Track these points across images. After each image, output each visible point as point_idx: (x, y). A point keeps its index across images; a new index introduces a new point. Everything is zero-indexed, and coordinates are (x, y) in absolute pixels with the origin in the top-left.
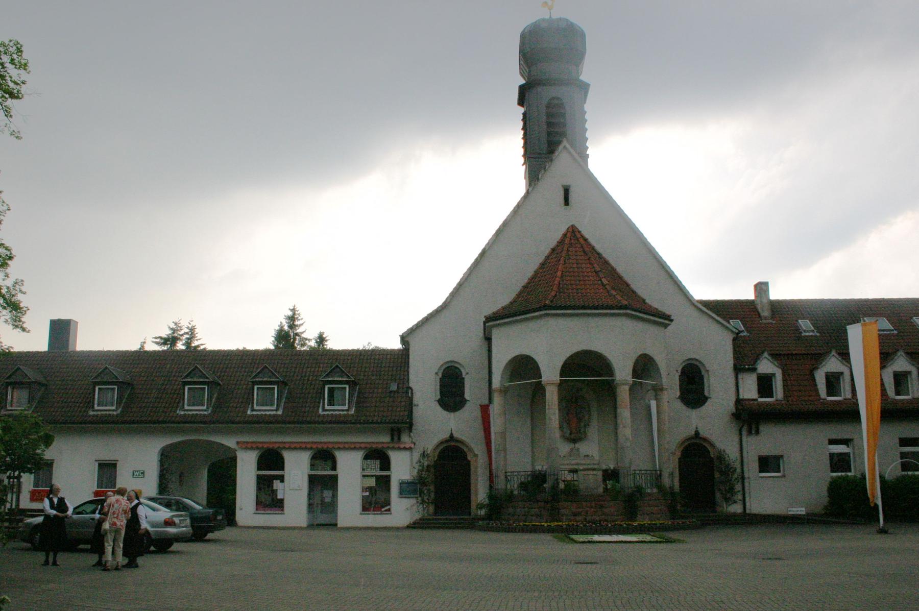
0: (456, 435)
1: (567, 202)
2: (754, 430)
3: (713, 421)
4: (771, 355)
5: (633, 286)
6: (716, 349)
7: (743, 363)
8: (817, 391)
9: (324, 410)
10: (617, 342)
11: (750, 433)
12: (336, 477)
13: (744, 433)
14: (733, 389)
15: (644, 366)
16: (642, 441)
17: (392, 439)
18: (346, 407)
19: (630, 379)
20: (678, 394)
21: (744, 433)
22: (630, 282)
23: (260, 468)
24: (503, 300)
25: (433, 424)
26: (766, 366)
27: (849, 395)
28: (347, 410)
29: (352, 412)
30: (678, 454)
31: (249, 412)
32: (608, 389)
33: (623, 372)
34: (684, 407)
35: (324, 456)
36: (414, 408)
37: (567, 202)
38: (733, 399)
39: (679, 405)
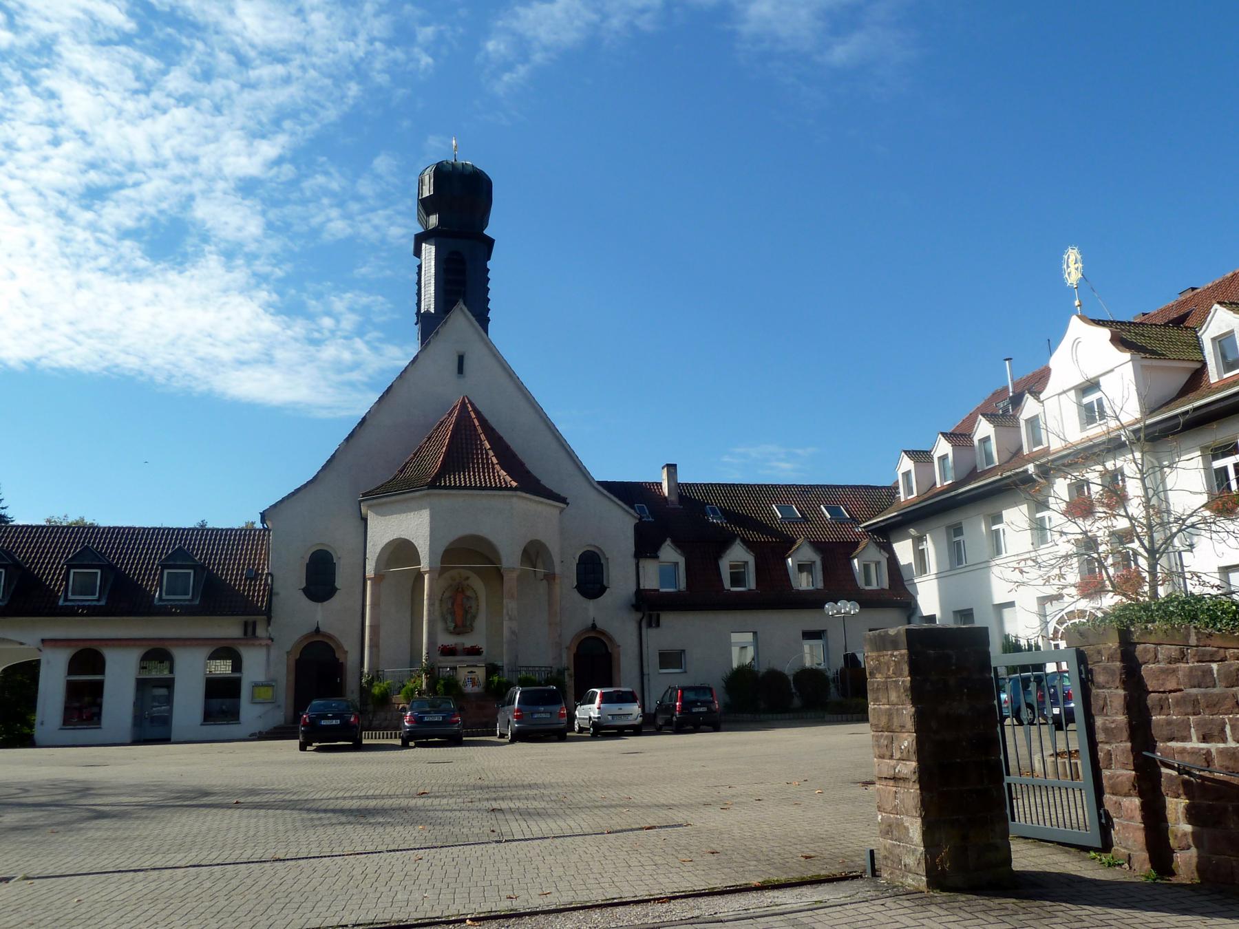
0: (599, 625)
1: (461, 359)
2: (654, 623)
3: (610, 613)
4: (673, 542)
5: (529, 466)
6: (617, 529)
7: (646, 547)
8: (721, 580)
9: (66, 599)
10: (506, 520)
11: (650, 625)
12: (172, 680)
13: (644, 624)
14: (634, 578)
15: (534, 553)
16: (527, 631)
17: (245, 633)
18: (189, 597)
19: (517, 565)
20: (575, 584)
21: (644, 624)
22: (524, 461)
23: (71, 671)
24: (384, 476)
25: (298, 615)
26: (669, 553)
27: (365, 742)
28: (98, 600)
29: (103, 603)
30: (574, 649)
31: (61, 602)
32: (495, 575)
33: (510, 558)
34: (582, 598)
35: (158, 654)
36: (274, 599)
37: (461, 359)
38: (633, 588)
39: (577, 596)
